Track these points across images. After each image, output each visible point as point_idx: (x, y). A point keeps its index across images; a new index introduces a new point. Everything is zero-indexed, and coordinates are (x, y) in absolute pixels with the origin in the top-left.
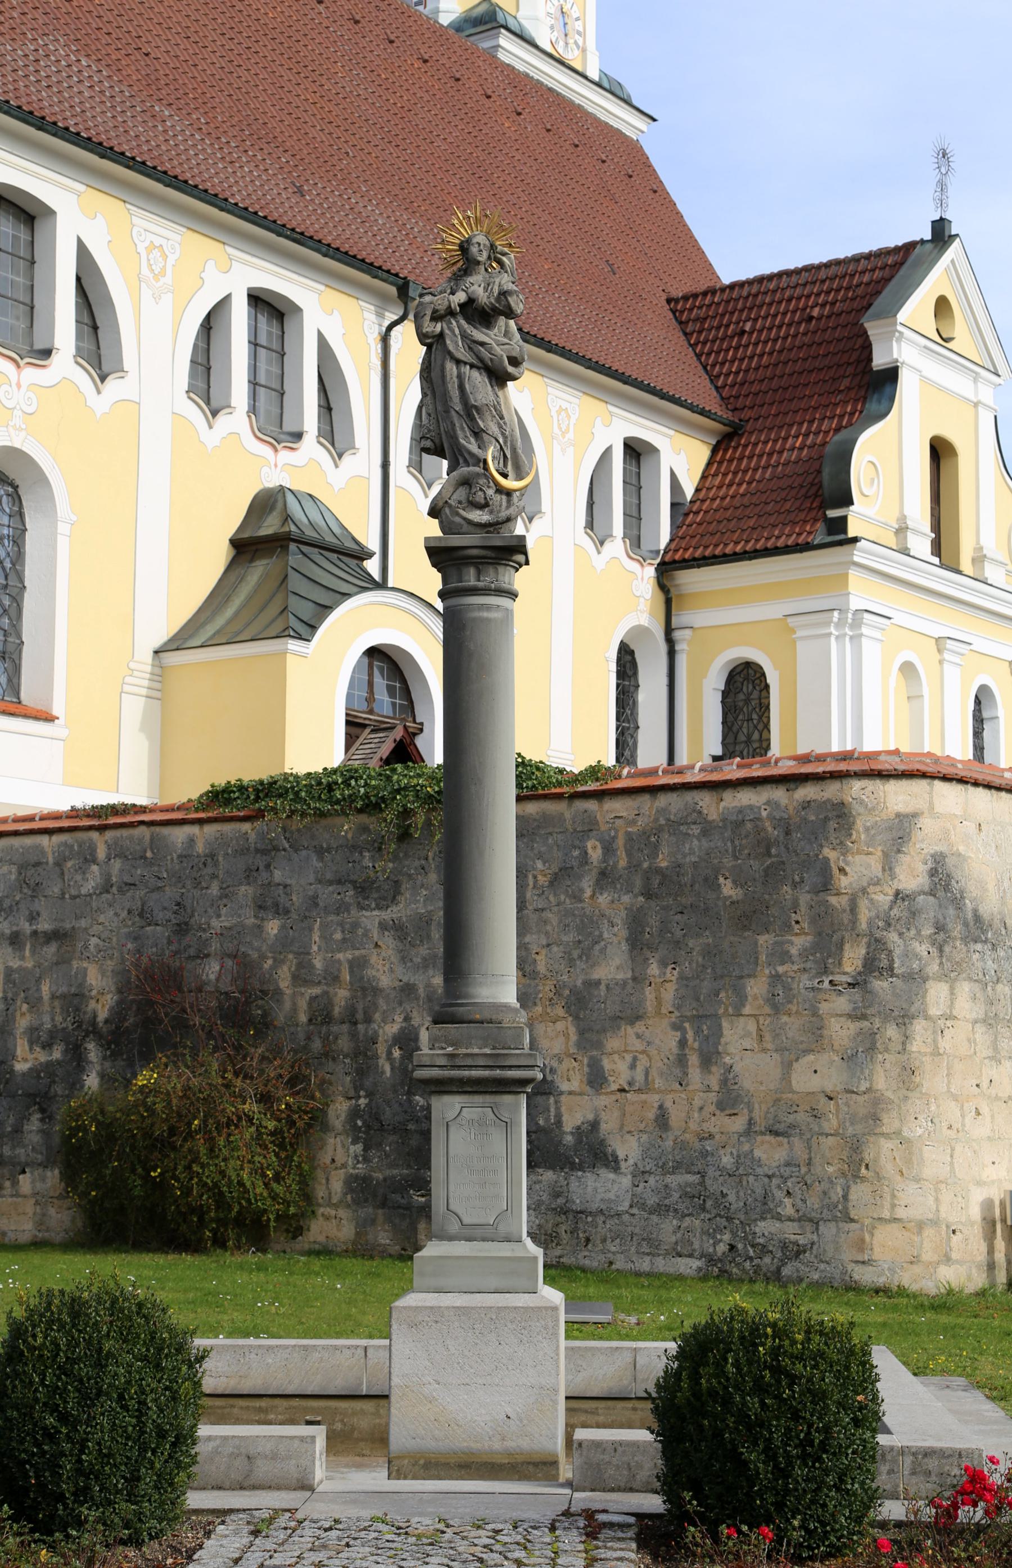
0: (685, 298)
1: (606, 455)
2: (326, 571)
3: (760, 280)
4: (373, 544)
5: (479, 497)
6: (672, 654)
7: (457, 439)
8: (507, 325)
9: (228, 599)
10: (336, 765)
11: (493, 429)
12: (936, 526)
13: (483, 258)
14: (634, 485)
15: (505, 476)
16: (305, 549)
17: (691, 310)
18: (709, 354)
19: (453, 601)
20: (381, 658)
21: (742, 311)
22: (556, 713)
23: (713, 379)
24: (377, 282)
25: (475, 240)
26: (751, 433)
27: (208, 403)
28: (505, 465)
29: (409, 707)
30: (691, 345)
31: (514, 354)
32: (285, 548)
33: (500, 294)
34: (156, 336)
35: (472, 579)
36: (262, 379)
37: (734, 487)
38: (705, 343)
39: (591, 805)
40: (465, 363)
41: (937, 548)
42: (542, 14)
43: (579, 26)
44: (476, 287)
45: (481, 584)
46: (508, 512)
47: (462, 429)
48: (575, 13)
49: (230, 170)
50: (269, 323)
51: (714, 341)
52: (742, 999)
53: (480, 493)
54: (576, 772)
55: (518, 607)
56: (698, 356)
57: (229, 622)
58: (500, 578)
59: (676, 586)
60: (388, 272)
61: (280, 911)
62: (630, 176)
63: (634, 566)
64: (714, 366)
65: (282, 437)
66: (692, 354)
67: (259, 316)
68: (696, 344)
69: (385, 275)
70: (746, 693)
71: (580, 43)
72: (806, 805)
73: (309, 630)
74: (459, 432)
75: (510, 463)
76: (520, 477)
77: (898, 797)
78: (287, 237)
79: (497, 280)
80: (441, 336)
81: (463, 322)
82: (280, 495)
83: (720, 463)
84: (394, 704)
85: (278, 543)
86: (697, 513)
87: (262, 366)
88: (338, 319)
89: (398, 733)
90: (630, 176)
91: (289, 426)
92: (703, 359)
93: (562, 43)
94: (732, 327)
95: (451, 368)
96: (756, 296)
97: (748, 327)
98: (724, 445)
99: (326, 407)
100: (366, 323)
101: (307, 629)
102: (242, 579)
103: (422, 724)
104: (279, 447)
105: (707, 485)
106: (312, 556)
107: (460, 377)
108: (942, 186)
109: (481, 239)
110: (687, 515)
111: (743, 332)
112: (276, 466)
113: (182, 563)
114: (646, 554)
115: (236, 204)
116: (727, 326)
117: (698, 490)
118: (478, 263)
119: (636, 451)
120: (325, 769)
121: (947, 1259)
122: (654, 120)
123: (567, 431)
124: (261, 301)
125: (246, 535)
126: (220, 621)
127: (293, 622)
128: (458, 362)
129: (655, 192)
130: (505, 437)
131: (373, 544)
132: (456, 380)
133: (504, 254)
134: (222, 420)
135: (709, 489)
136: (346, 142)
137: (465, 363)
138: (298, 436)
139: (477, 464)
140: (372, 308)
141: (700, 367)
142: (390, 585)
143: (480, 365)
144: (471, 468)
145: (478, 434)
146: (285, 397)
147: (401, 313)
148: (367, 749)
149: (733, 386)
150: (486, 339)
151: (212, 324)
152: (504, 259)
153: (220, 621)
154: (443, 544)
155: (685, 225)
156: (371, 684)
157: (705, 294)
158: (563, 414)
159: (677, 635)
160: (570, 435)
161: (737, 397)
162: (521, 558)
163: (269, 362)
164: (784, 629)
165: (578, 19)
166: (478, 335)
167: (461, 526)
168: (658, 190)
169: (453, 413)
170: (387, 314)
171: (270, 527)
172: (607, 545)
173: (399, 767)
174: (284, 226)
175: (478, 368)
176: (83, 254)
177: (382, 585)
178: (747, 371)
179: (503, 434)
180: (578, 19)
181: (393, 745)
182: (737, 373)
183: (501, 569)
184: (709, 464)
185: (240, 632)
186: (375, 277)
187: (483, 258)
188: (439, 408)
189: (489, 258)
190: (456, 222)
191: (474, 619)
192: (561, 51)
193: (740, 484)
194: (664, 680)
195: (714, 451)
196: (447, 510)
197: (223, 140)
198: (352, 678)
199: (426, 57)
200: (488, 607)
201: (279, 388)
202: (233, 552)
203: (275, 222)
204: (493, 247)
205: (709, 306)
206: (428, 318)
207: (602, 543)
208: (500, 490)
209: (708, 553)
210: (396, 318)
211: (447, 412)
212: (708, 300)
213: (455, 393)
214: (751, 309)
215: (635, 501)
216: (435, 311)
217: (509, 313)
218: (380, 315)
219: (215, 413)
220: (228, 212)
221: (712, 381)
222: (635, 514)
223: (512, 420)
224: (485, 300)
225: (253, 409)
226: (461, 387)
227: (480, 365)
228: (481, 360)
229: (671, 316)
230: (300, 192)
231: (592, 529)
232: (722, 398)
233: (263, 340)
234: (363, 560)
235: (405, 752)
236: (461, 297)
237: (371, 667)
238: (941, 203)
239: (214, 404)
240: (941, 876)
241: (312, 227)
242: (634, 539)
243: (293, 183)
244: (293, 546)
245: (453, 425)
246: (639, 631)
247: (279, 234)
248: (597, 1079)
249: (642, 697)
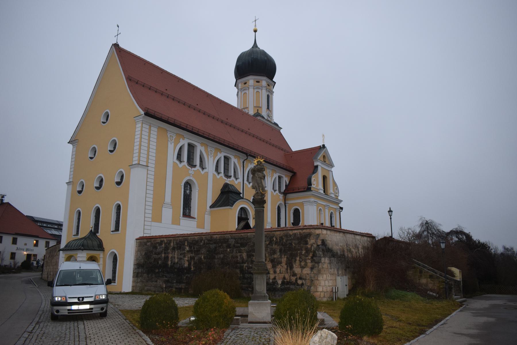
1: (276, 178)
6: (286, 207)
12: (324, 188)
20: (243, 210)
22: (270, 221)
34: (210, 165)
39: (274, 232)
41: (324, 192)
52: (296, 260)
61: (230, 248)
70: (297, 214)
72: (304, 233)
77: (318, 231)
99: (235, 172)
101: (232, 205)
108: (323, 140)
113: (211, 195)
121: (324, 297)
126: (219, 203)
131: (241, 192)
138: (231, 176)
153: (219, 203)
164: (302, 204)
171: (227, 190)
176: (201, 152)
177: (243, 198)
235: (247, 226)
238: (323, 142)
240: (323, 242)
242: (280, 192)
248: (275, 272)
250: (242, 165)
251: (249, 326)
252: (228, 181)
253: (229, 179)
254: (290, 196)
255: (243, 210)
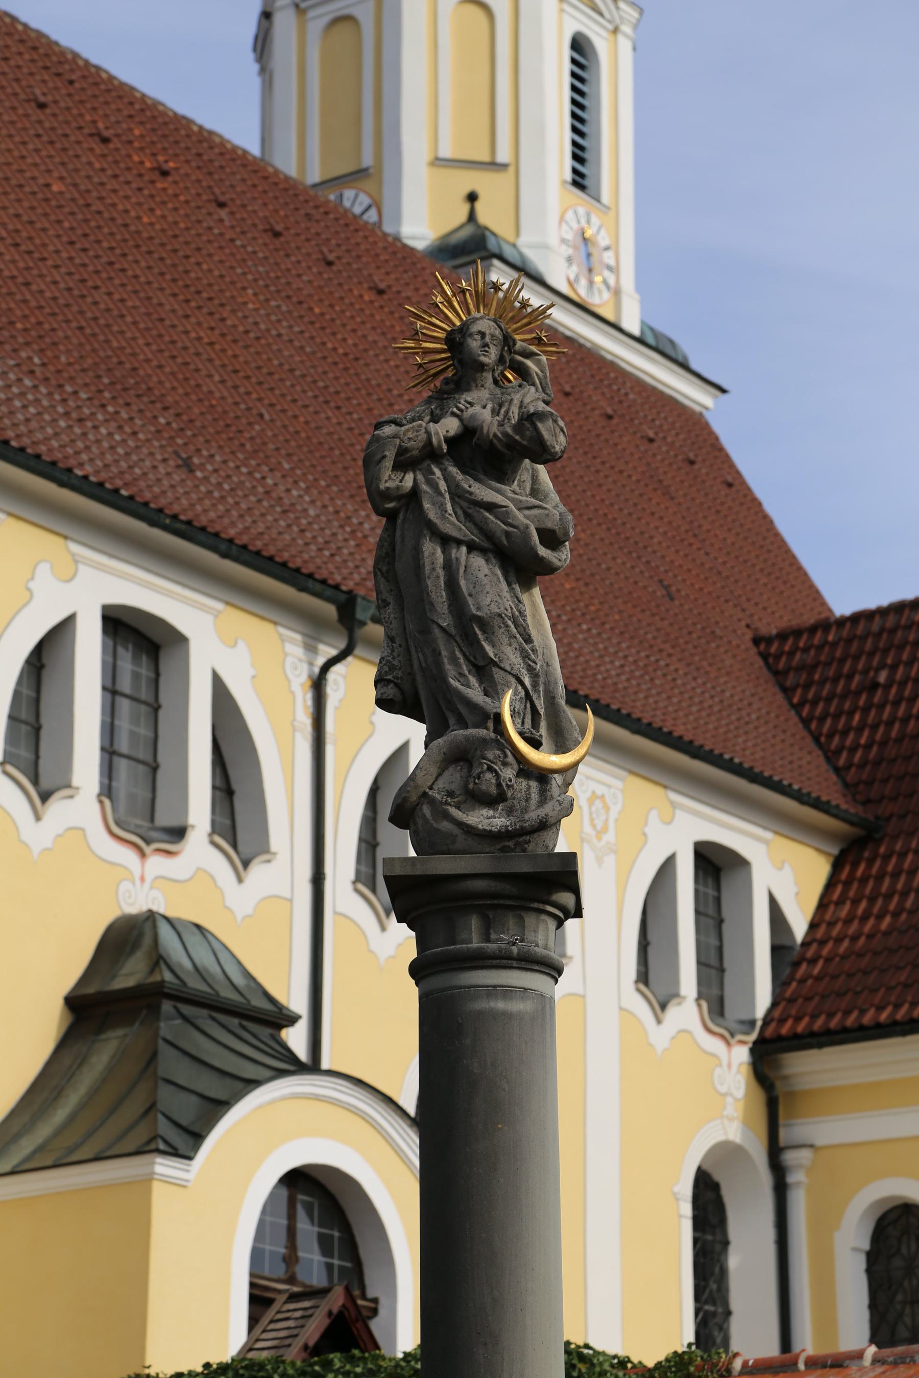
0: (782, 636)
1: (667, 868)
2: (218, 1046)
3: (899, 608)
4: (297, 1001)
5: (488, 782)
6: (781, 1190)
7: (445, 680)
8: (535, 479)
9: (58, 1094)
10: (227, 1358)
11: (513, 659)
13: (491, 357)
14: (712, 918)
15: (536, 744)
16: (187, 1010)
17: (792, 653)
18: (822, 720)
19: (437, 982)
20: (317, 1197)
21: (871, 654)
23: (831, 757)
24: (306, 599)
25: (474, 328)
26: (895, 837)
27: (35, 781)
28: (535, 724)
29: (354, 1275)
30: (793, 706)
31: (549, 525)
32: (155, 1011)
33: (521, 419)
35: (475, 937)
36: (123, 745)
37: (871, 922)
38: (814, 703)
40: (459, 543)
42: (553, 241)
43: (609, 258)
44: (477, 409)
45: (492, 947)
46: (542, 812)
47: (454, 660)
48: (603, 240)
49: (77, 431)
50: (136, 659)
51: (829, 700)
53: (489, 776)
54: (650, 1364)
55: (563, 988)
56: (806, 722)
57: (59, 1132)
58: (529, 935)
59: (785, 1078)
60: (324, 582)
62: (692, 463)
63: (715, 1045)
64: (830, 736)
65: (154, 834)
66: (796, 719)
67: (120, 650)
68: (802, 704)
69: (318, 587)
71: (612, 281)
73: (191, 1141)
74: (449, 668)
75: (543, 724)
76: (561, 747)
78: (165, 528)
79: (517, 398)
80: (414, 494)
81: (453, 470)
82: (148, 925)
83: (847, 884)
84: (329, 1267)
85: (146, 1001)
86: (813, 961)
87: (124, 724)
88: (240, 653)
89: (336, 1300)
90: (692, 463)
91: (164, 818)
92: (814, 725)
93: (583, 282)
94: (857, 678)
95: (432, 552)
96: (893, 631)
97: (882, 677)
98: (850, 861)
99: (225, 790)
100: (289, 660)
101: (187, 1140)
102: (83, 1061)
103: (375, 1301)
104: (148, 849)
105: (828, 917)
106: (199, 1022)
107: (450, 567)
109: (486, 325)
110: (796, 964)
111: (875, 685)
112: (142, 879)
114: (734, 1026)
115: (86, 477)
116: (850, 677)
117: (813, 926)
118: (482, 367)
119: (714, 864)
120: (207, 1365)
122: (724, 391)
123: (605, 830)
124: (121, 625)
125: (91, 990)
126: (44, 1131)
127: (164, 1127)
128: (446, 541)
129: (730, 485)
130: (534, 675)
131: (298, 1003)
132: (441, 573)
133: (530, 355)
134: (57, 808)
135: (831, 924)
136: (260, 399)
137: (459, 543)
138: (178, 833)
139: (482, 725)
140: (298, 637)
141: (809, 740)
142: (325, 1065)
143: (486, 544)
144: (471, 731)
145: (484, 669)
146: (160, 774)
147: (342, 645)
148: (281, 1329)
149: (862, 766)
150: (498, 499)
151: (46, 659)
152: (529, 363)
153: (44, 1131)
154: (418, 871)
155: (777, 534)
156: (291, 1232)
157: (813, 630)
158: (598, 804)
159: (790, 1158)
160: (610, 837)
161: (870, 783)
162: (567, 899)
163: (135, 719)
165: (607, 248)
166: (484, 492)
167: (454, 838)
168: (734, 483)
169: (437, 631)
170: (322, 647)
171: (131, 974)
172: (673, 1012)
173: (336, 1359)
174: (161, 511)
175: (483, 551)
177: (313, 1067)
178: (883, 744)
179: (531, 670)
180: (607, 248)
181: (327, 1322)
182: (868, 747)
183: (530, 919)
184: (829, 886)
185: (77, 1147)
186: (303, 589)
187: (491, 357)
188: (411, 626)
189: (501, 360)
190: (439, 299)
191: (480, 1013)
192: (582, 292)
193: (880, 917)
194: (770, 1234)
195: (837, 865)
196: (426, 810)
197: (69, 389)
198: (261, 1224)
199: (382, 286)
200: (507, 992)
201: (149, 759)
202: (69, 1019)
203: (146, 504)
204: (507, 341)
205: (820, 648)
206: (388, 463)
207: (663, 1006)
208: (527, 770)
209: (834, 1024)
210: (333, 652)
211: (425, 631)
212: (818, 638)
213: (440, 597)
214: (886, 651)
215: (714, 942)
216: (402, 451)
217: (541, 453)
218: (311, 649)
219: (45, 797)
220: (73, 488)
221: (828, 759)
222: (714, 961)
223: (546, 646)
224: (495, 429)
225: (107, 791)
226: (452, 585)
227: (486, 544)
228: (488, 535)
229: (760, 662)
230: (187, 466)
231: (646, 984)
232: (846, 785)
233: (125, 685)
234: (280, 1027)
236: (450, 426)
237: (292, 1204)
239: (45, 783)
241: (206, 514)
242: (716, 1002)
243: (176, 453)
244: (167, 1006)
245: (437, 654)
246: (725, 1152)
247: (153, 523)
249: (734, 1261)
250: (305, 721)
251: (539, 707)
252: (149, 884)
253: (157, 864)
254: (810, 1067)
255: (317, 1197)
